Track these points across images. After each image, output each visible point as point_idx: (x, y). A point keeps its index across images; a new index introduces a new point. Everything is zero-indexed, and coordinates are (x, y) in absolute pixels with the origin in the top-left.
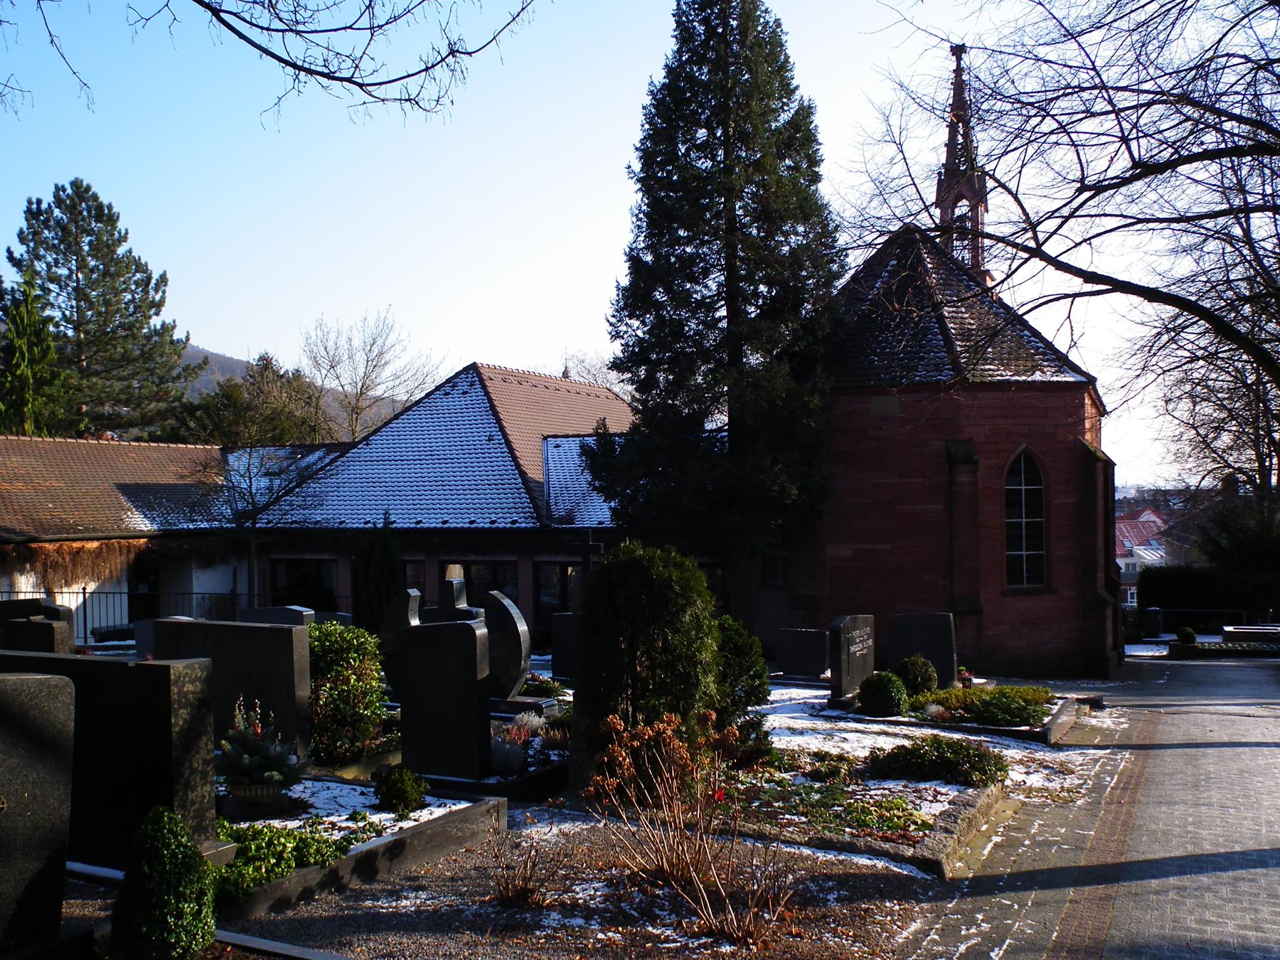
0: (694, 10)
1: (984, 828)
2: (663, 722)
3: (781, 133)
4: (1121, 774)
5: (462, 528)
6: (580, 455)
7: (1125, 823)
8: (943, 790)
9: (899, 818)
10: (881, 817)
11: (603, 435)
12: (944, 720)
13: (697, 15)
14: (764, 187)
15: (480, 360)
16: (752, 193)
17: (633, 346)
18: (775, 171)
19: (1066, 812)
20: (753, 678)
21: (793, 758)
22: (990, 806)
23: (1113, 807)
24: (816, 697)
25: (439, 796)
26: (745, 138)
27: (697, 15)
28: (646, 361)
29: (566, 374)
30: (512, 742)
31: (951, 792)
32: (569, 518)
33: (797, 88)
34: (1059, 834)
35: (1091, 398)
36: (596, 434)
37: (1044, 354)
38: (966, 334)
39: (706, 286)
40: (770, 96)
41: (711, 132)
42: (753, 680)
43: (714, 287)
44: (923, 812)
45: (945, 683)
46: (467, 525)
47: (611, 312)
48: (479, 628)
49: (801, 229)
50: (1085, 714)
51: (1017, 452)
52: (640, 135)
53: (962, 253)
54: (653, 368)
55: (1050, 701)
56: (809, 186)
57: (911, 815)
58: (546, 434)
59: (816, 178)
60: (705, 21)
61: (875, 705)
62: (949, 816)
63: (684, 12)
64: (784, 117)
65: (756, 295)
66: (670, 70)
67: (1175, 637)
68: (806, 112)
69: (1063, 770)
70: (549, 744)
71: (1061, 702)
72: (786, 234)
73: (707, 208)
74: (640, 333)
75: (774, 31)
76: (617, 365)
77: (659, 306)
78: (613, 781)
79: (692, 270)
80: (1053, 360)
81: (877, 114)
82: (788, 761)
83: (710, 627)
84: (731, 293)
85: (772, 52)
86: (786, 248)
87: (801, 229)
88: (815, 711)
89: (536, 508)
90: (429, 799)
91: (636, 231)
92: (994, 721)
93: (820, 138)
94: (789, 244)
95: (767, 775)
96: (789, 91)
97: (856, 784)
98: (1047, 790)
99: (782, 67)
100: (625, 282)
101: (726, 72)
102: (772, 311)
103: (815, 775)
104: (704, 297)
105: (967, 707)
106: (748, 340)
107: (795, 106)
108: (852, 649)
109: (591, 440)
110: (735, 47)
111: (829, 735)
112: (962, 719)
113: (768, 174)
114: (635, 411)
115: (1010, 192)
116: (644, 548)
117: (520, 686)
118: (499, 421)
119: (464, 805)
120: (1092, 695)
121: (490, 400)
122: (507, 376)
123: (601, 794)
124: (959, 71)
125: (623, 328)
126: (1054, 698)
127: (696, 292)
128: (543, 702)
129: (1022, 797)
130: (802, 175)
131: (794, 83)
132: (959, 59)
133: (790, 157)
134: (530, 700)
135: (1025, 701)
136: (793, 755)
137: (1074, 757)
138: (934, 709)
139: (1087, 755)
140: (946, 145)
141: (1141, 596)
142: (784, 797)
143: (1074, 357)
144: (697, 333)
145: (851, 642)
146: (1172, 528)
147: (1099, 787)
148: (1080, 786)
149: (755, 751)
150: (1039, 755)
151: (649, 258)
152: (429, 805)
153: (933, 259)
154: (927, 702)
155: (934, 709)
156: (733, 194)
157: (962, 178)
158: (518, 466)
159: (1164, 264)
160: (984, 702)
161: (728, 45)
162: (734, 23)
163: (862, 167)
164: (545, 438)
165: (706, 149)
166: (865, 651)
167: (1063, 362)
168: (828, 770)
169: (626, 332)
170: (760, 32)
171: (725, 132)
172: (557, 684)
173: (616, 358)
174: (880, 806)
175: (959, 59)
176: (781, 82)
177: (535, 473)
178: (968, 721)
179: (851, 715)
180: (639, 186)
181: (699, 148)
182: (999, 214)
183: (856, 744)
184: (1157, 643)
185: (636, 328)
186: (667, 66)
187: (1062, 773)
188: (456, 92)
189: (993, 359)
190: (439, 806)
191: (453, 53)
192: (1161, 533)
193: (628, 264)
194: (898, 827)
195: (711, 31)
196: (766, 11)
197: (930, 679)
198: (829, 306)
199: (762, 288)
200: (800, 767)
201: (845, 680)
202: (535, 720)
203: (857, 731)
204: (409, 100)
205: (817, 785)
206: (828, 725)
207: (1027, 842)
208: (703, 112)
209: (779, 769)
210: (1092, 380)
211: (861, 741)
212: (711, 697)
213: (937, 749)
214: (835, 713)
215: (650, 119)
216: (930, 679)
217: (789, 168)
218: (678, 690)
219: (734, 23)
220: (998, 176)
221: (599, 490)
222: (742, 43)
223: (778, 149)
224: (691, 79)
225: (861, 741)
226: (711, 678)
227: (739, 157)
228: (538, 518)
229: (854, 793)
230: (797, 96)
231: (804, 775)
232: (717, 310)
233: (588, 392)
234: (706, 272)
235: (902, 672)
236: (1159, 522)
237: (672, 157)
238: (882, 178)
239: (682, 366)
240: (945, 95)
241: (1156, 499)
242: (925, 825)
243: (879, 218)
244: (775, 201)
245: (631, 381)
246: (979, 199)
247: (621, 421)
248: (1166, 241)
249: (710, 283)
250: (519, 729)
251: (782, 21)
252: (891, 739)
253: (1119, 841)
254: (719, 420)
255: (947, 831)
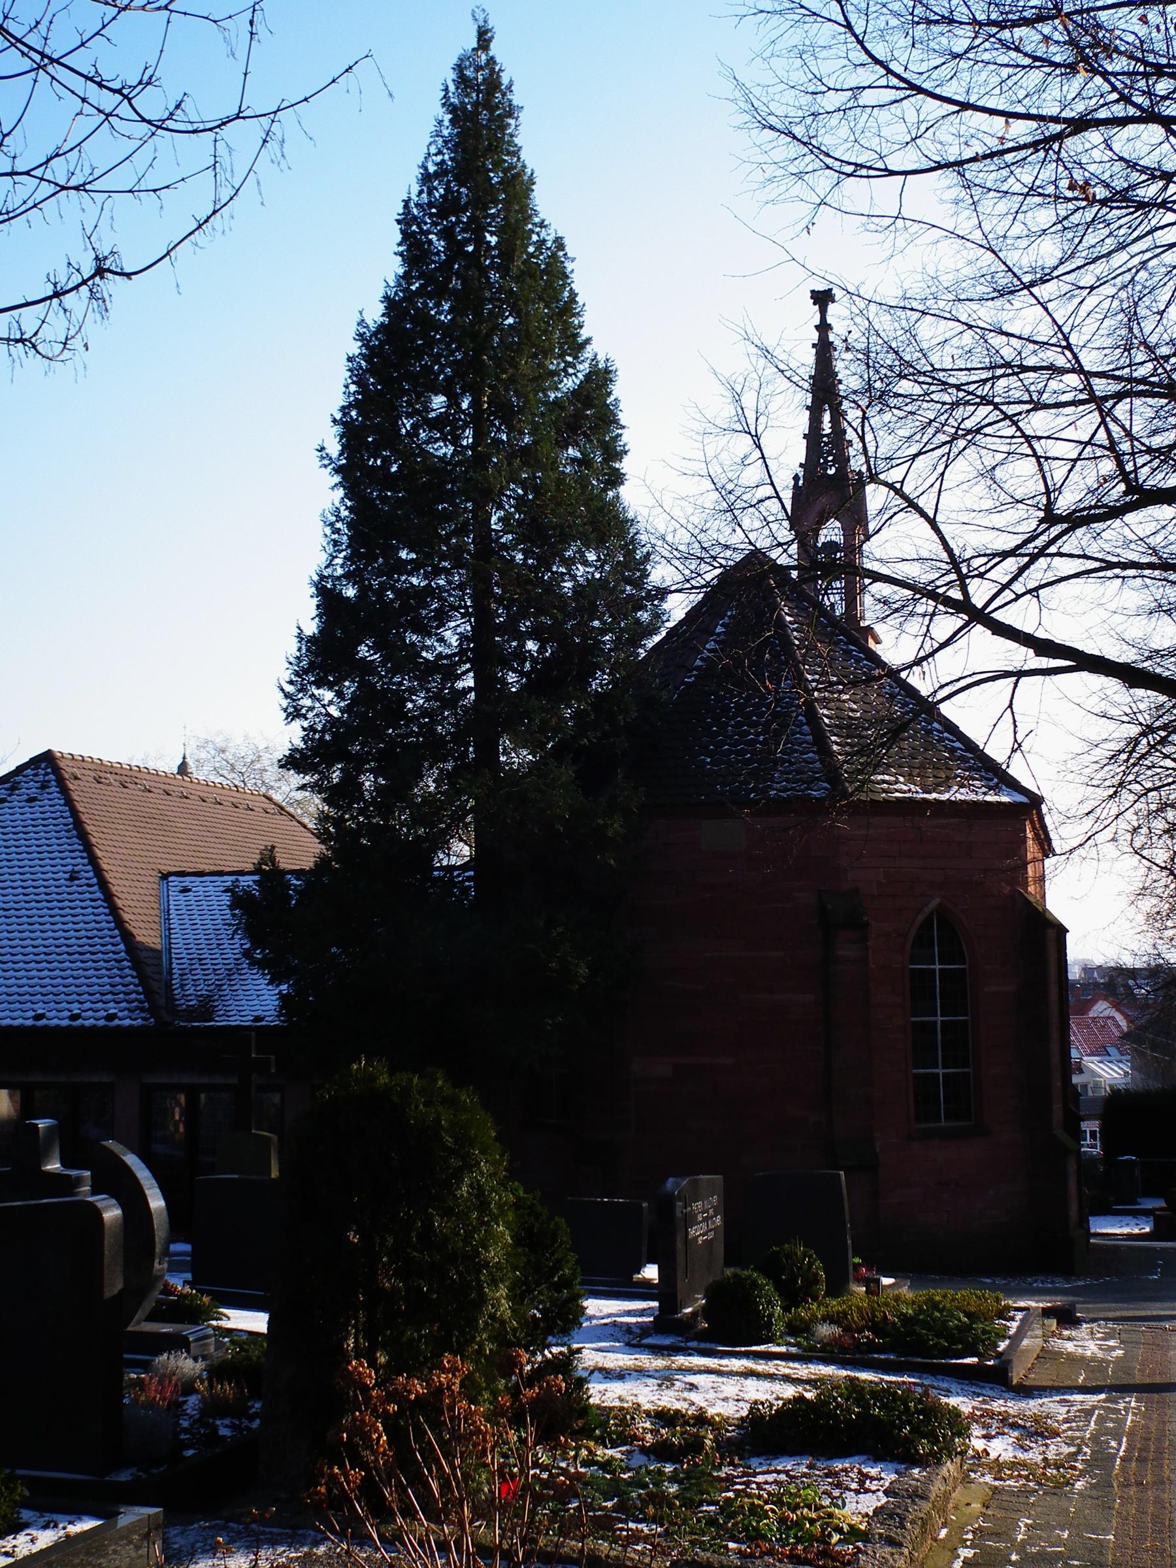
0: (431, 215)
1: (943, 1533)
2: (444, 1370)
3: (563, 408)
4: (1131, 1435)
5: (21, 1028)
6: (232, 907)
7: (1156, 1519)
8: (873, 1472)
9: (812, 1522)
10: (782, 1520)
11: (270, 874)
12: (844, 1350)
13: (435, 224)
14: (536, 490)
15: (61, 746)
16: (518, 498)
17: (323, 731)
18: (554, 464)
19: (1064, 1503)
20: (558, 1287)
21: (623, 1422)
22: (947, 1496)
23: (1132, 1491)
24: (629, 1313)
25: (41, 1509)
26: (507, 414)
27: (435, 224)
28: (344, 756)
29: (183, 768)
30: (151, 1405)
31: (884, 1475)
32: (206, 1009)
33: (588, 341)
34: (1059, 1542)
35: (1034, 828)
36: (257, 871)
37: (964, 760)
38: (848, 728)
39: (442, 640)
40: (547, 353)
41: (453, 401)
42: (559, 1291)
43: (454, 641)
44: (847, 1511)
45: (837, 1288)
46: (30, 1022)
47: (287, 675)
48: (107, 1208)
49: (591, 556)
50: (1053, 1335)
51: (927, 911)
52: (342, 401)
53: (834, 600)
54: (355, 766)
55: (1003, 1313)
56: (605, 490)
57: (830, 1515)
58: (166, 869)
59: (616, 479)
60: (447, 234)
61: (730, 1327)
62: (891, 1516)
63: (415, 218)
64: (569, 383)
65: (521, 655)
66: (390, 303)
67: (1161, 1204)
68: (601, 378)
69: (1039, 1430)
70: (213, 1408)
71: (1019, 1316)
72: (569, 563)
73: (446, 517)
74: (334, 711)
75: (554, 256)
76: (294, 761)
77: (366, 667)
78: (357, 1474)
79: (421, 613)
80: (978, 770)
81: (722, 390)
82: (615, 1426)
83: (500, 1206)
84: (483, 652)
85: (549, 285)
86: (568, 585)
87: (591, 556)
88: (633, 1338)
89: (148, 993)
90: (26, 1515)
91: (330, 549)
92: (927, 1352)
93: (623, 418)
94: (573, 578)
95: (584, 1452)
96: (575, 345)
97: (731, 1464)
98: (1024, 1464)
99: (567, 311)
100: (311, 628)
101: (478, 314)
102: (548, 681)
103: (662, 1451)
104: (440, 656)
105: (879, 1327)
106: (509, 726)
107: (584, 368)
108: (693, 1232)
109: (247, 881)
110: (494, 276)
111: (666, 1379)
112: (871, 1347)
113: (543, 468)
114: (322, 836)
115: (923, 514)
116: (391, 1074)
117: (148, 1306)
118: (88, 847)
119: (87, 1525)
120: (1058, 1301)
121: (74, 813)
122: (102, 772)
123: (339, 1501)
124: (824, 327)
125: (307, 702)
126: (1008, 1308)
127: (427, 648)
128: (190, 1331)
129: (988, 1479)
130: (596, 473)
131: (584, 334)
132: (823, 312)
133: (576, 444)
134: (166, 1329)
135: (967, 1315)
136: (625, 1414)
137: (1051, 1406)
138: (825, 1330)
139: (1070, 1404)
140: (805, 436)
141: (1106, 1135)
142: (615, 1489)
143: (1017, 770)
144: (424, 712)
145: (689, 1220)
146: (1143, 1028)
147: (1101, 1460)
148: (1073, 1456)
149: (563, 1412)
150: (997, 1406)
151: (350, 592)
152: (27, 1525)
153: (789, 603)
154: (814, 1320)
155: (825, 1330)
156: (487, 496)
157: (830, 488)
158: (119, 923)
159: (1137, 629)
160: (903, 1317)
161: (484, 271)
162: (493, 240)
163: (701, 468)
164: (165, 876)
165: (445, 426)
166: (711, 1236)
167: (996, 774)
168: (682, 1437)
169: (311, 709)
170: (532, 255)
171: (475, 404)
172: (206, 1299)
173: (294, 750)
174: (779, 1503)
175: (823, 312)
176: (563, 331)
177: (147, 935)
178: (881, 1349)
179: (693, 1344)
180: (337, 479)
181: (438, 424)
182: (896, 545)
183: (711, 1395)
184: (1136, 1214)
185: (328, 702)
186: (386, 298)
187: (1041, 1435)
188: (93, 329)
189: (889, 766)
190: (45, 1527)
191: (100, 272)
192: (1126, 1036)
193: (315, 601)
194: (812, 1538)
195: (455, 248)
196: (542, 225)
197: (816, 1281)
198: (632, 675)
199: (531, 646)
200: (635, 1437)
201: (681, 1284)
202: (187, 1365)
203: (709, 1371)
204: (21, 341)
205: (669, 1469)
206: (660, 1363)
207: (1014, 1557)
208: (441, 371)
209: (601, 1441)
210: (1036, 801)
211: (727, 1389)
212: (503, 1323)
213: (858, 1403)
214: (667, 1341)
215: (359, 377)
216: (816, 1281)
217: (574, 460)
218: (447, 1312)
219: (493, 240)
220: (907, 489)
221: (261, 964)
222: (504, 270)
223: (558, 432)
224: (426, 323)
225: (727, 1389)
226: (503, 1291)
227: (497, 442)
228: (153, 1011)
229: (730, 1480)
230: (588, 353)
231: (644, 1450)
232: (459, 677)
233: (231, 803)
234: (442, 618)
235: (771, 1269)
236: (1123, 1023)
237: (390, 438)
238: (730, 487)
239: (400, 769)
240: (807, 359)
241: (1115, 982)
242: (853, 1534)
243: (727, 547)
244: (553, 512)
245: (316, 787)
246: (856, 519)
247: (302, 852)
248: (1136, 594)
249: (448, 634)
250: (161, 1382)
251: (566, 241)
252: (766, 1385)
253: (1155, 1550)
254: (461, 851)
255: (891, 1542)
